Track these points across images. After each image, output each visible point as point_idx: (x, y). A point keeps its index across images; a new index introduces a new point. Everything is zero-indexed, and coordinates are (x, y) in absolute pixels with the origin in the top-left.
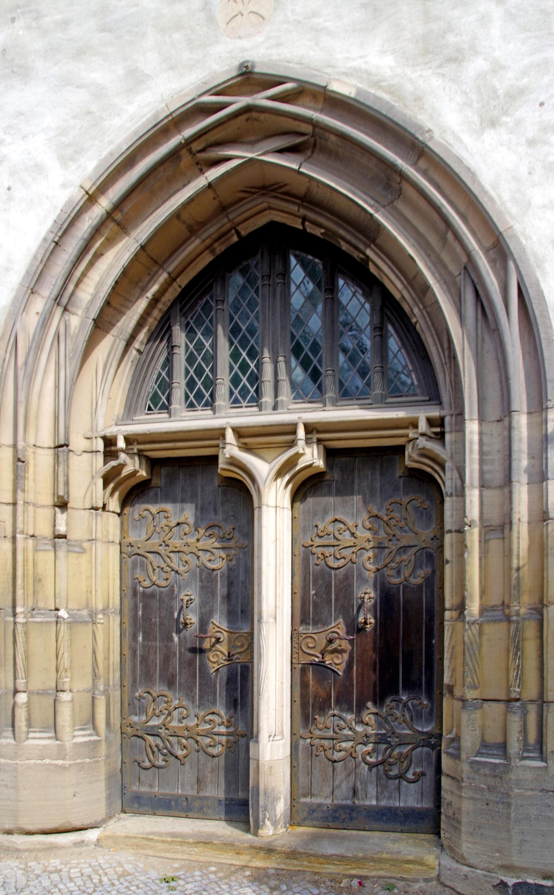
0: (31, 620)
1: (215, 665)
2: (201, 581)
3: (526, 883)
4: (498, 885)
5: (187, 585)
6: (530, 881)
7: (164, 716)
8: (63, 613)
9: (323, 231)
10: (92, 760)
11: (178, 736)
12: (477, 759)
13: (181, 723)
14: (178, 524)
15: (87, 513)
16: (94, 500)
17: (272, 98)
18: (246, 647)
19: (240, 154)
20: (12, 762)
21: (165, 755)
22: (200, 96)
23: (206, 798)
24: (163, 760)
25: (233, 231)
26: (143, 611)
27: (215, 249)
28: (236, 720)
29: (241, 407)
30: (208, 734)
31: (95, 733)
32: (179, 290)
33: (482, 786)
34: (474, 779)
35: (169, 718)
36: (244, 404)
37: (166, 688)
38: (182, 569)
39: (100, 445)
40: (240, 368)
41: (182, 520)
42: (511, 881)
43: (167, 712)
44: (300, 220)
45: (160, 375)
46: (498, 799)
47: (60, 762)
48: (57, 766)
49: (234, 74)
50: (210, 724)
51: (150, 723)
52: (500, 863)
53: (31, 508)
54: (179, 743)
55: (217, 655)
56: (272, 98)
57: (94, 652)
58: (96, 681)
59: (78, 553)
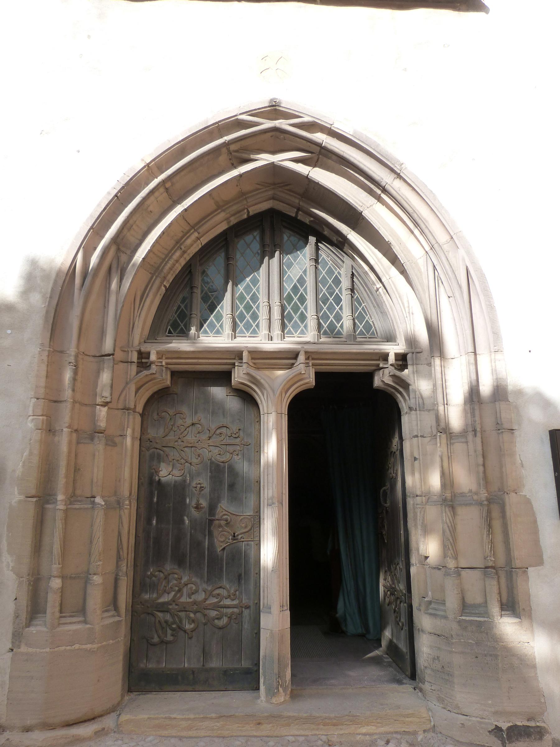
0: (69, 506)
1: (222, 544)
2: (211, 472)
3: (516, 726)
4: (493, 730)
5: (199, 474)
6: (519, 724)
7: (173, 593)
8: (98, 500)
9: (312, 219)
10: (114, 641)
11: (186, 611)
12: (464, 618)
13: (190, 598)
14: (193, 424)
15: (119, 412)
16: (127, 402)
17: (293, 125)
18: (249, 527)
19: (264, 159)
20: (42, 651)
21: (173, 630)
22: (240, 114)
23: (212, 669)
24: (172, 635)
25: (246, 211)
26: (157, 499)
27: (230, 221)
28: (241, 593)
29: (246, 337)
30: (216, 607)
31: (116, 614)
32: (200, 246)
33: (470, 641)
34: (462, 636)
35: (178, 595)
36: (248, 335)
37: (176, 567)
38: (195, 461)
39: (134, 357)
40: (245, 308)
41: (195, 421)
42: (504, 726)
43: (177, 588)
44: (296, 210)
45: (179, 307)
46: (486, 652)
47: (89, 646)
48: (86, 650)
49: (267, 105)
50: (217, 598)
51: (161, 600)
52: (493, 710)
53: (77, 405)
54: (188, 617)
55: (223, 535)
56: (293, 125)
57: (120, 535)
58: (120, 563)
59: (112, 446)
